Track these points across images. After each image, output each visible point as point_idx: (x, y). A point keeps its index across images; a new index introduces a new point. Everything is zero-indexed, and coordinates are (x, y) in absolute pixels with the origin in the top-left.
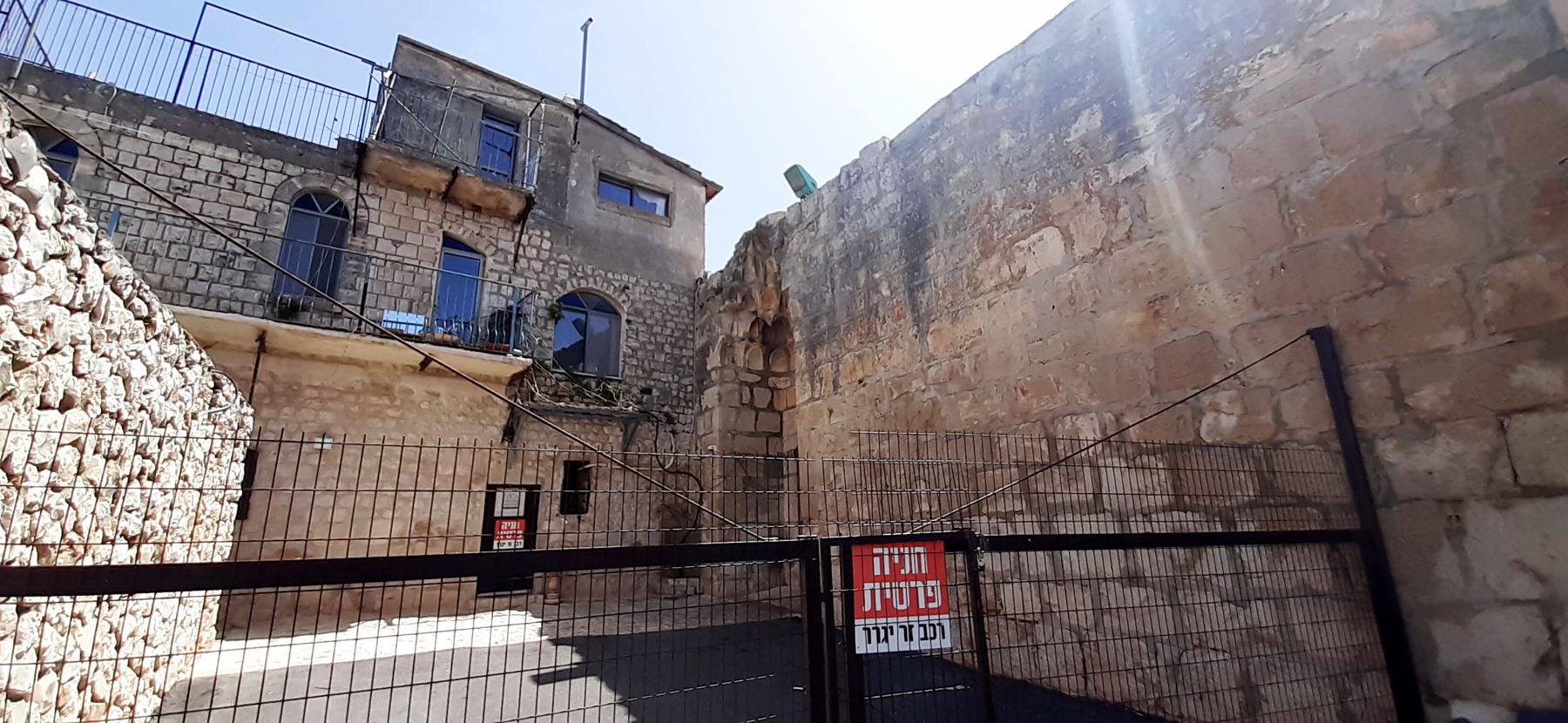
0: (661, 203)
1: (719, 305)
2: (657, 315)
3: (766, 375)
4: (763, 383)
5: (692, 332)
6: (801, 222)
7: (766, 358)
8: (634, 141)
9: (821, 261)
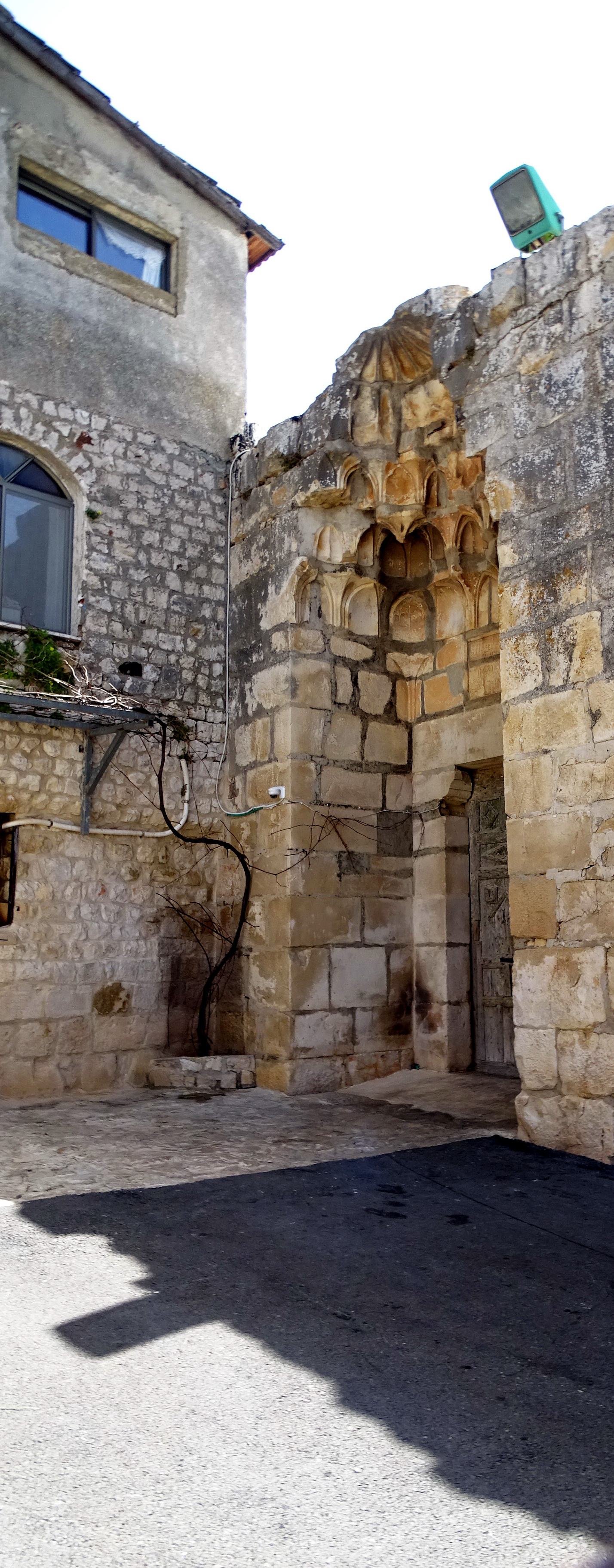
0: (153, 259)
1: (289, 491)
2: (152, 507)
3: (383, 645)
4: (376, 662)
5: (222, 550)
6: (524, 301)
7: (384, 609)
8: (94, 102)
9: (579, 389)
